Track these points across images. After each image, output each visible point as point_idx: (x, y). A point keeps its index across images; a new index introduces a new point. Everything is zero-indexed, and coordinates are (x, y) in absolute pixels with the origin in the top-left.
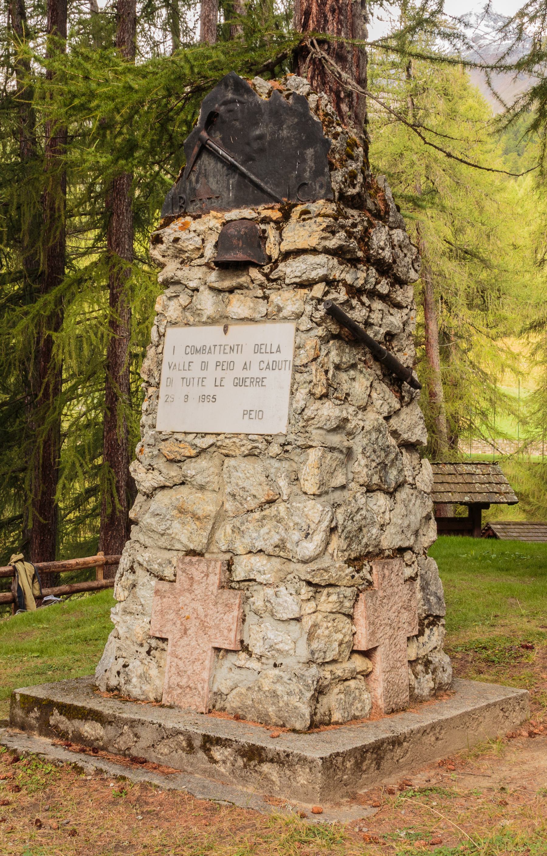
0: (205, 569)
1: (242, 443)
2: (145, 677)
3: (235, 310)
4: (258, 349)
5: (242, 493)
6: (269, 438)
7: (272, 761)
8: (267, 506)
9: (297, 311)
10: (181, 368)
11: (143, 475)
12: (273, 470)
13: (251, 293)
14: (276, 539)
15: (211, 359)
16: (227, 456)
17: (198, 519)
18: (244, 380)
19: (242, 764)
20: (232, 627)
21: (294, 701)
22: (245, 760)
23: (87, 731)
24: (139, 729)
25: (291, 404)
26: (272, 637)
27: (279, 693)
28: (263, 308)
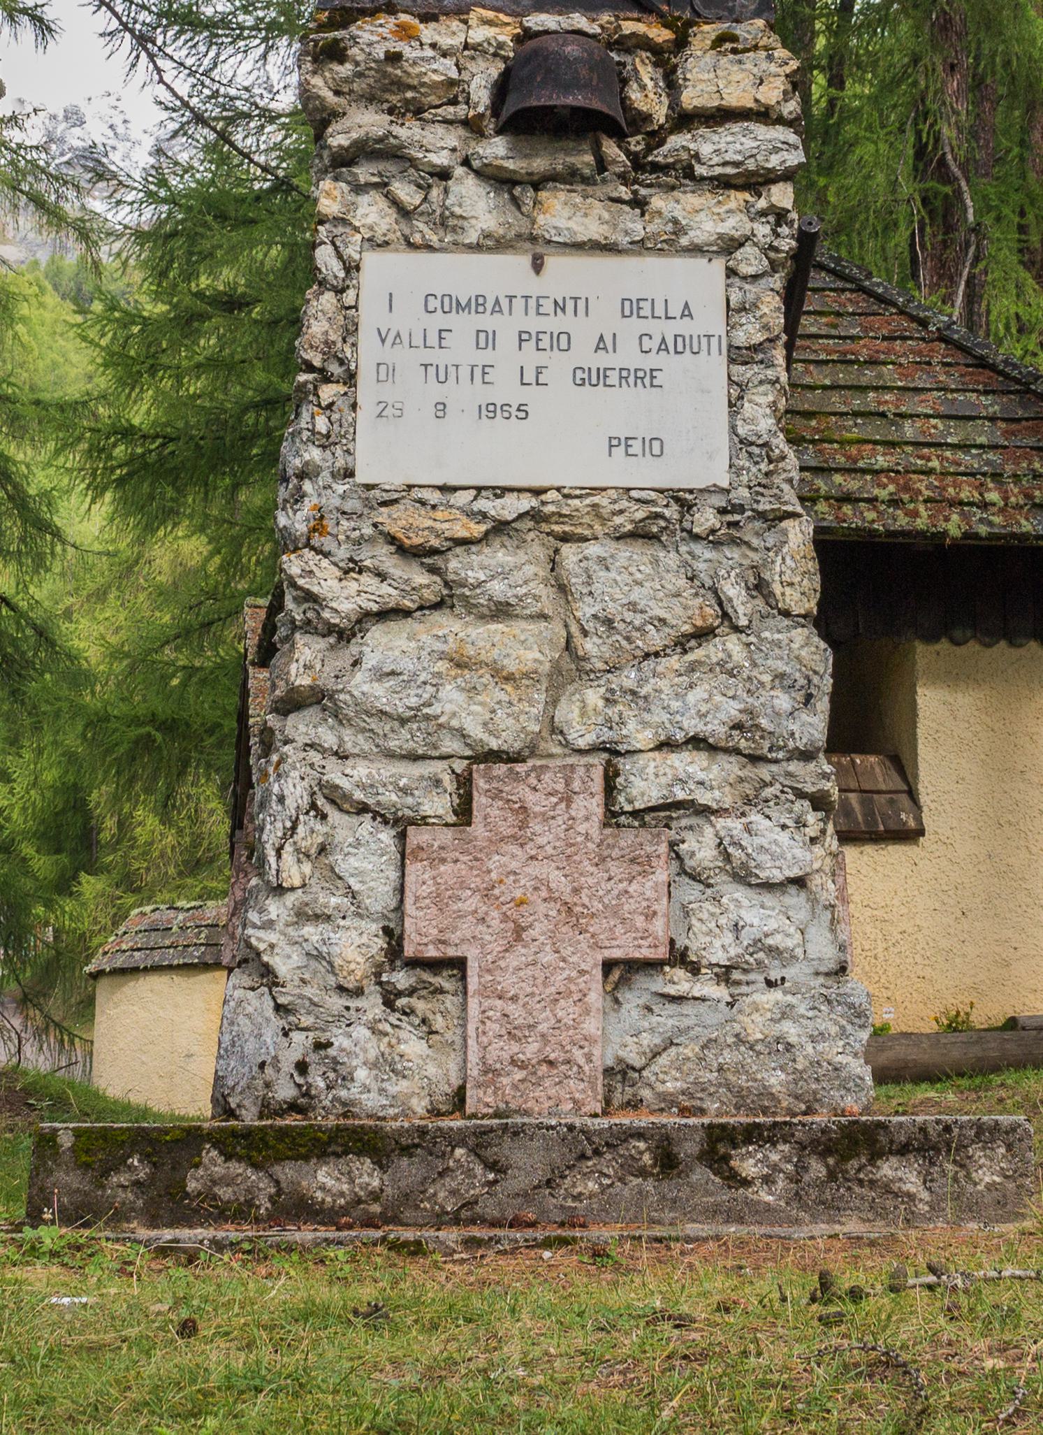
0: (560, 787)
1: (617, 507)
2: (389, 1065)
3: (562, 223)
4: (632, 308)
5: (629, 616)
6: (688, 496)
7: (903, 1150)
8: (693, 643)
9: (737, 234)
10: (418, 341)
11: (334, 583)
12: (701, 566)
13: (600, 191)
14: (732, 710)
15: (506, 327)
16: (565, 538)
17: (509, 678)
18: (603, 374)
19: (823, 1172)
20: (656, 907)
21: (833, 1051)
22: (831, 1161)
23: (322, 1188)
24: (507, 1150)
25: (733, 429)
26: (756, 922)
27: (793, 1039)
28: (635, 226)
